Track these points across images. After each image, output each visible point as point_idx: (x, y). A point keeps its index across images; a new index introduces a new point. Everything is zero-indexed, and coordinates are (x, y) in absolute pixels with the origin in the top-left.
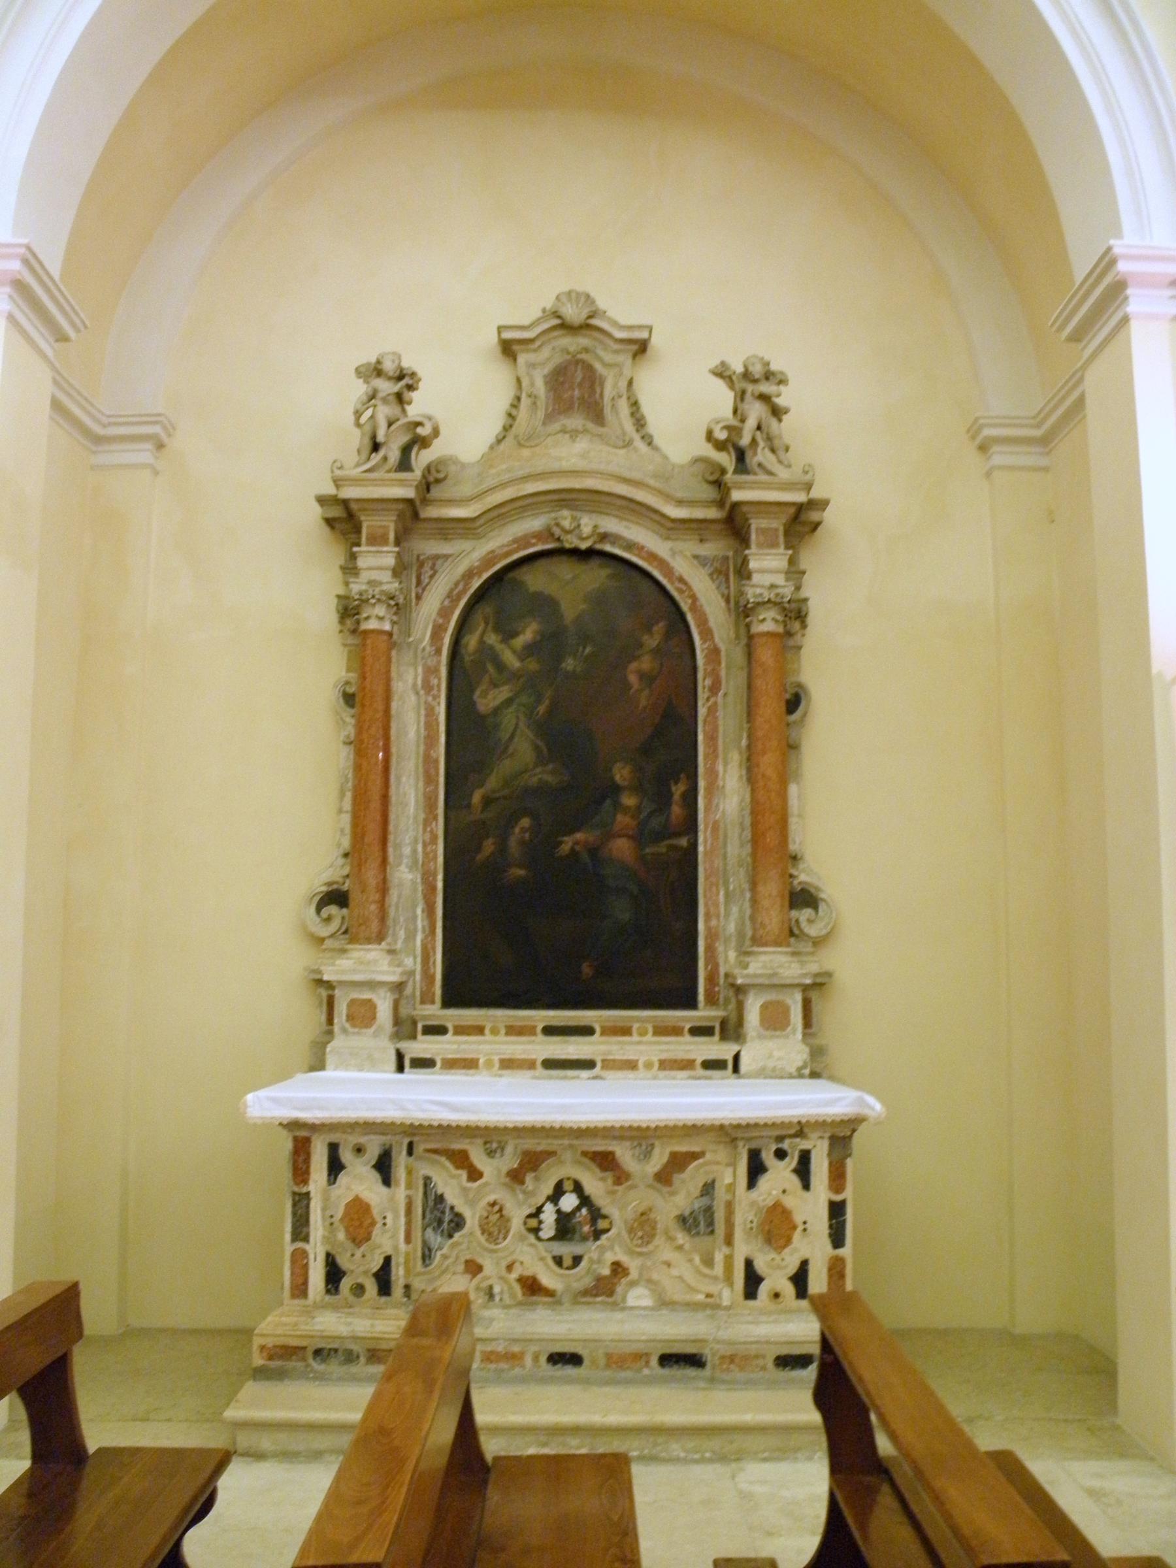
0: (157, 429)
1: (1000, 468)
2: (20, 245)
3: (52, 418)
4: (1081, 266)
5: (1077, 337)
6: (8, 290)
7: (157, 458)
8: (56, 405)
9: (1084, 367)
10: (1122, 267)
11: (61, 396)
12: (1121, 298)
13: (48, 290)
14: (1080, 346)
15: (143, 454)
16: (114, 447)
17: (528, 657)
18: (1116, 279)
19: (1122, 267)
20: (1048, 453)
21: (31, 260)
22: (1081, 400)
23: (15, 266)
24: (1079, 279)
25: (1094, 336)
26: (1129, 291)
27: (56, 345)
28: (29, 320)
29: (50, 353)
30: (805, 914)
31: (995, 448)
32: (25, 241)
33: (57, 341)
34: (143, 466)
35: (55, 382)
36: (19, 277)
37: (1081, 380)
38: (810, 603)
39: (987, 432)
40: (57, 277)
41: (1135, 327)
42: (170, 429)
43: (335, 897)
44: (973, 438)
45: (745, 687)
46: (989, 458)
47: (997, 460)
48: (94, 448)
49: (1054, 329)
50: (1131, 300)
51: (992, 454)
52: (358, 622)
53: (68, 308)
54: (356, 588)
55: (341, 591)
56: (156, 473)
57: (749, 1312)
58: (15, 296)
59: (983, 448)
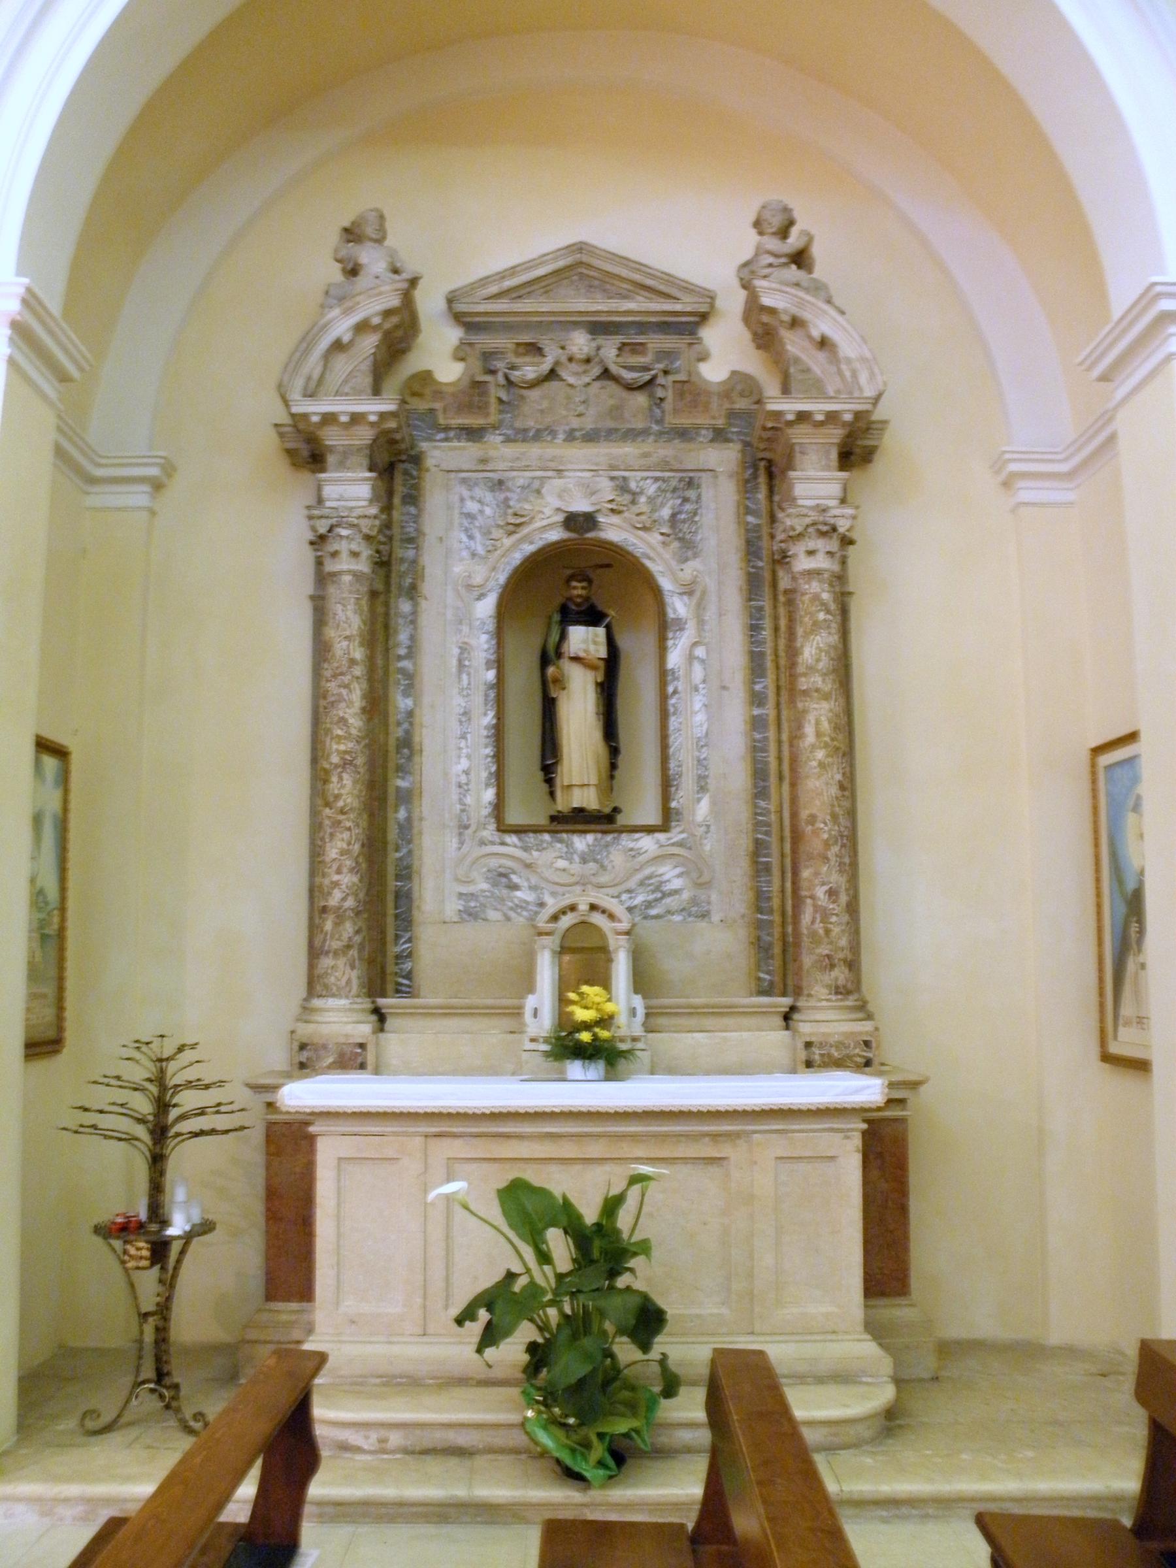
0: (154, 472)
3: (55, 465)
5: (1105, 378)
8: (59, 452)
9: (1116, 408)
11: (66, 445)
13: (51, 332)
17: (623, 1052)
21: (30, 301)
22: (1112, 438)
24: (1117, 311)
25: (1148, 357)
28: (42, 374)
31: (1022, 484)
35: (59, 429)
36: (18, 318)
37: (1111, 419)
38: (854, 597)
39: (1014, 467)
44: (998, 472)
45: (136, 1285)
47: (1025, 496)
49: (1083, 367)
57: (480, 550)
58: (16, 338)
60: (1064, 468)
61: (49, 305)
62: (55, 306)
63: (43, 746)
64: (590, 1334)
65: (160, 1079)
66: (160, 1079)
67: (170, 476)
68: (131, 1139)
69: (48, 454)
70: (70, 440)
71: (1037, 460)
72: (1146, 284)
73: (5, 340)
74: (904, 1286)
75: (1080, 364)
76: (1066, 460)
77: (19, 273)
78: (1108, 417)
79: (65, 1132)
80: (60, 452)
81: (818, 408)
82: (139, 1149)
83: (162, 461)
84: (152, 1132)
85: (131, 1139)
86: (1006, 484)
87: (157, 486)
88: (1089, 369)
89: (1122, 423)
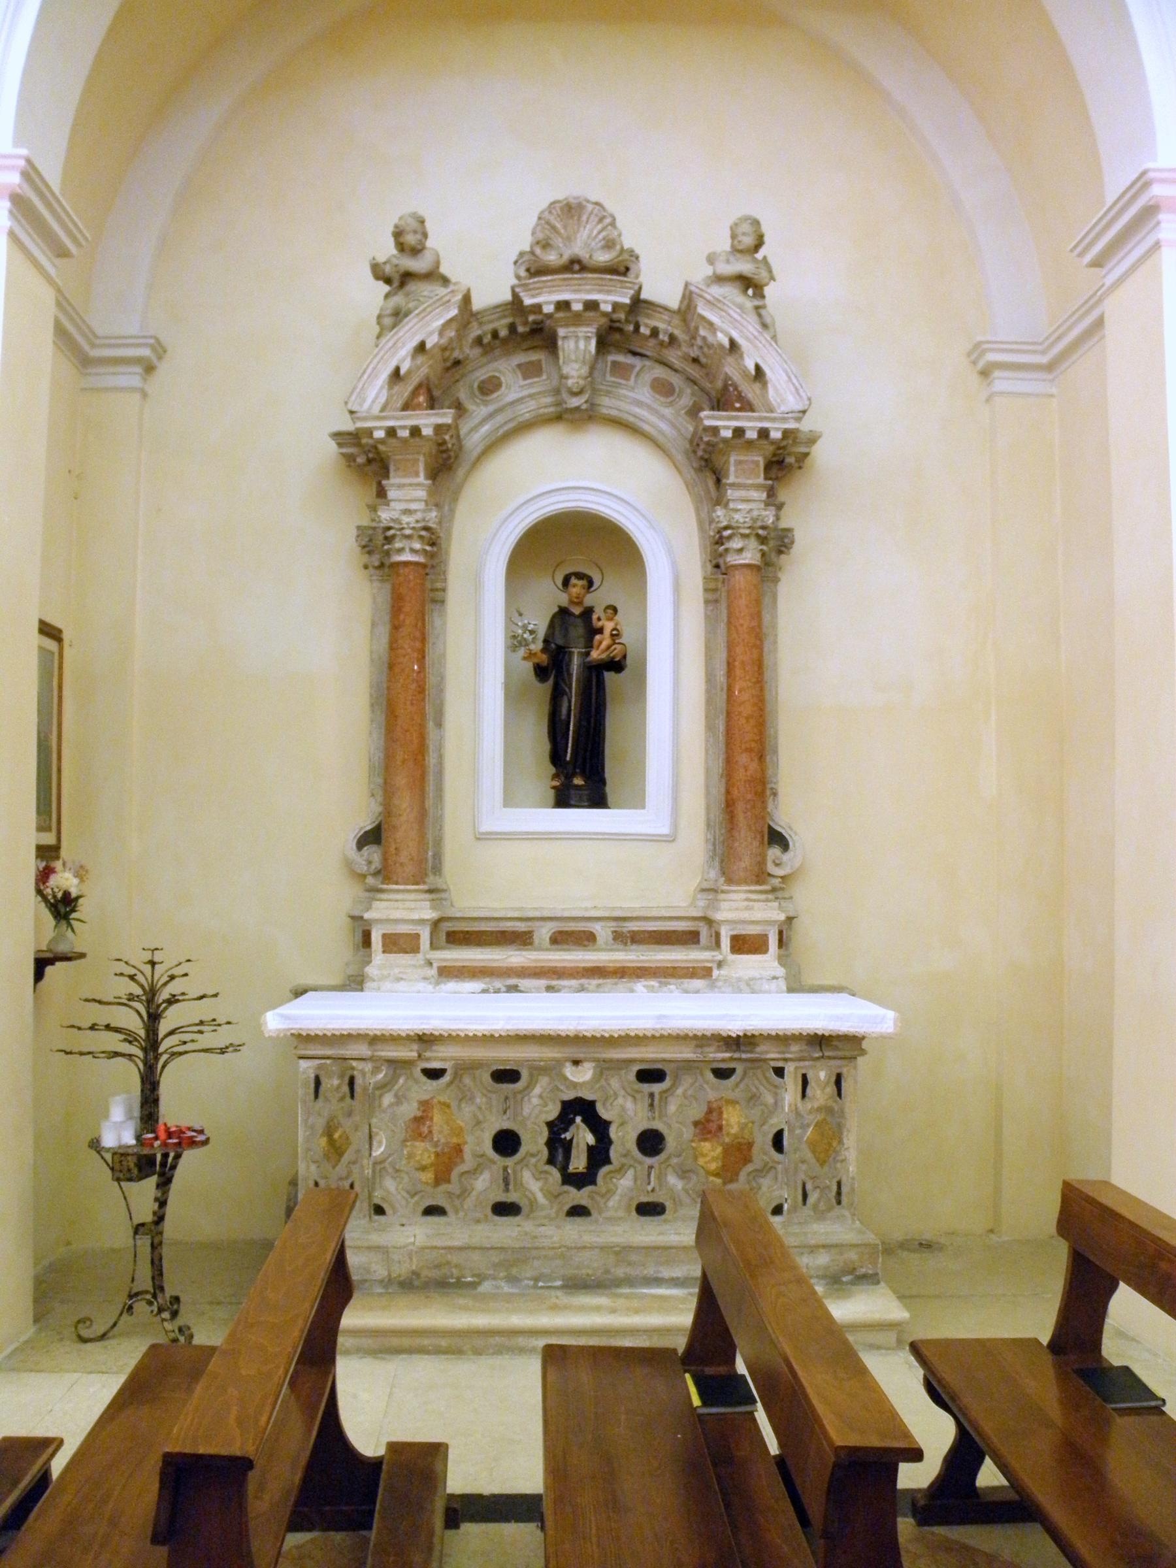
0: (146, 352)
1: (1002, 393)
2: (20, 157)
4: (1115, 184)
5: (1097, 263)
6: (7, 204)
7: (145, 380)
10: (1157, 191)
12: (1155, 220)
13: (48, 205)
14: (1104, 271)
15: (131, 378)
16: (102, 370)
18: (1151, 203)
19: (1157, 191)
20: (1052, 380)
21: (30, 173)
22: (1099, 323)
23: (14, 179)
24: (1110, 201)
26: (1162, 216)
27: (57, 261)
29: (52, 271)
30: (774, 852)
32: (24, 152)
33: (58, 256)
34: (133, 389)
35: (59, 304)
36: (19, 191)
39: (991, 357)
40: (57, 191)
41: (1166, 253)
42: (160, 349)
43: (372, 837)
46: (989, 384)
48: (1051, 377)
50: (1163, 225)
51: (994, 379)
52: (388, 553)
53: (1104, 222)
54: (385, 515)
55: (365, 522)
56: (145, 395)
59: (985, 373)
60: (1044, 360)
61: (51, 183)
62: (53, 175)
63: (48, 630)
64: (614, 939)
65: (151, 993)
66: (151, 993)
67: (160, 358)
68: (130, 1056)
69: (48, 335)
70: (71, 319)
71: (1011, 351)
72: (1140, 170)
73: (6, 213)
74: (891, 1038)
75: (1072, 251)
76: (1043, 352)
77: (17, 142)
78: (1097, 299)
79: (111, 1323)
80: (60, 332)
81: (751, 425)
82: (137, 1065)
83: (152, 341)
84: (144, 1050)
85: (130, 1056)
86: (985, 373)
87: (149, 369)
88: (1081, 255)
89: (1111, 307)
